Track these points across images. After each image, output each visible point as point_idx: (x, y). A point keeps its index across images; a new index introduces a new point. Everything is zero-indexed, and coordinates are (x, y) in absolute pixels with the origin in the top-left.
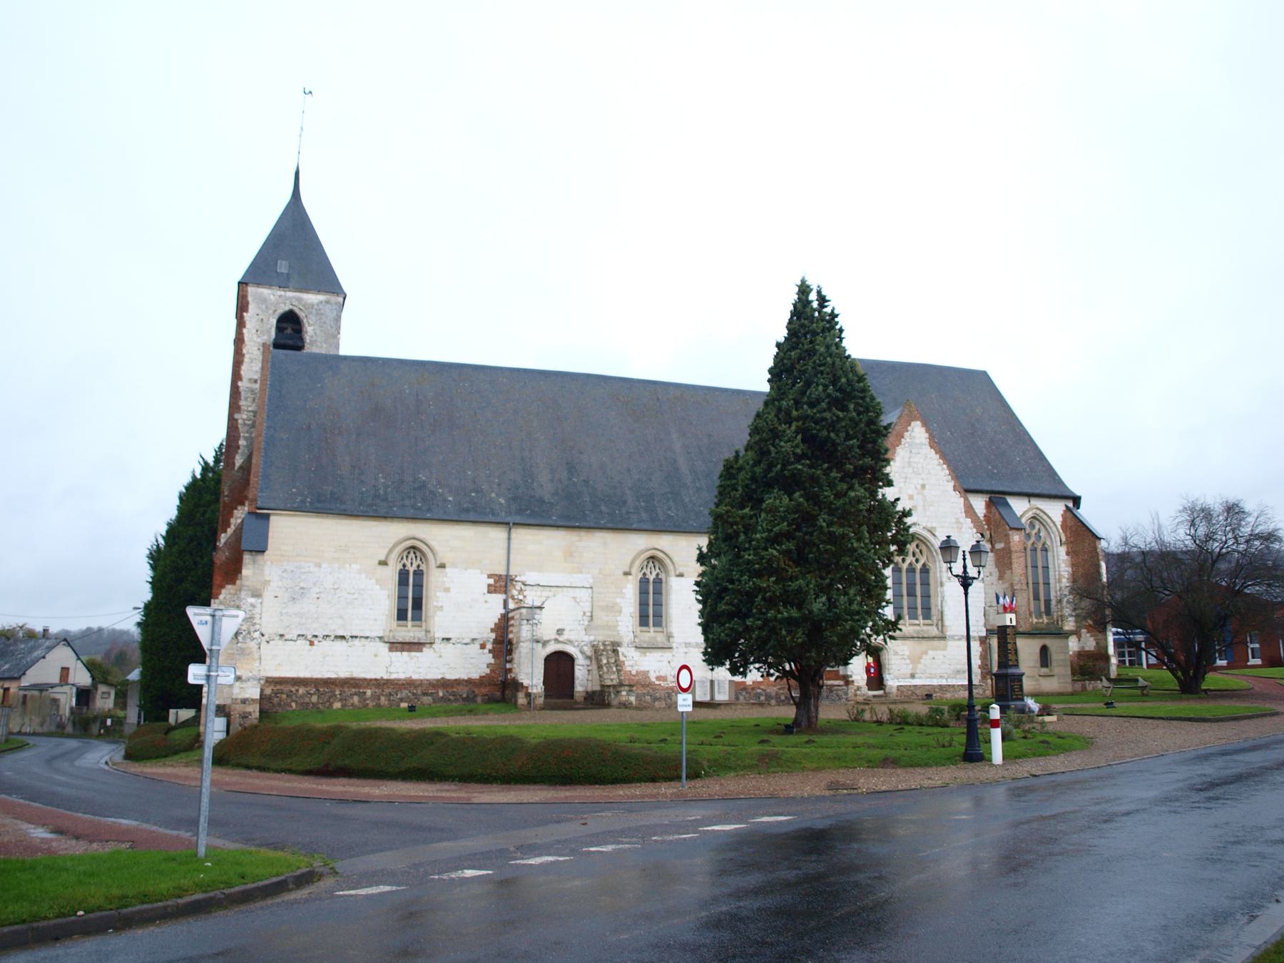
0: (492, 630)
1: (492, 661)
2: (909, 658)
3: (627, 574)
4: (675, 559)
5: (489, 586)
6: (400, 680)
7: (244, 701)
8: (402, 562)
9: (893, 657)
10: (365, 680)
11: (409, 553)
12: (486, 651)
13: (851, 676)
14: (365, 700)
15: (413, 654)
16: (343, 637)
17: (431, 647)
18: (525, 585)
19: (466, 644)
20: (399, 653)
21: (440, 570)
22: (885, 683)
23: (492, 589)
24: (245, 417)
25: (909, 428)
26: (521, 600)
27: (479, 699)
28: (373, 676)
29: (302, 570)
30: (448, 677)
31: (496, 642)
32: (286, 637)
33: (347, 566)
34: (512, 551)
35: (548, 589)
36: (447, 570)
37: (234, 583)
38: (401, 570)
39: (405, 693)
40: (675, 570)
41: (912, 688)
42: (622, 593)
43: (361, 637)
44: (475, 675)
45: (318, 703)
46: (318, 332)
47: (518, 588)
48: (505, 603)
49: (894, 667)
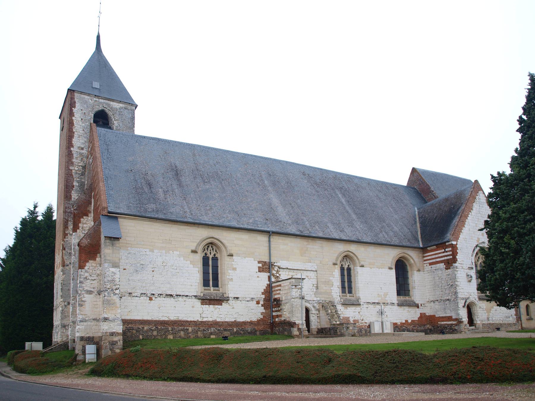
0: (263, 293)
1: (264, 311)
2: (486, 310)
3: (335, 264)
4: (359, 257)
5: (259, 267)
6: (209, 322)
7: (112, 334)
8: (205, 252)
9: (479, 309)
10: (187, 321)
11: (208, 247)
12: (260, 305)
13: (462, 319)
14: (188, 333)
15: (216, 306)
16: (171, 295)
17: (227, 303)
18: (279, 268)
19: (248, 301)
20: (207, 306)
21: (229, 257)
22: (475, 322)
23: (261, 270)
24: (77, 169)
25: (478, 194)
26: (278, 277)
27: (258, 333)
28: (192, 320)
29: (141, 253)
30: (238, 320)
31: (265, 300)
32: (134, 295)
33: (171, 252)
34: (272, 248)
35: (293, 271)
36: (234, 257)
37: (94, 259)
38: (204, 256)
39: (212, 329)
40: (360, 263)
41: (489, 325)
42: (332, 274)
43: (183, 296)
44: (254, 319)
45: (157, 335)
46: (121, 125)
47: (276, 269)
48: (269, 278)
49: (480, 314)
